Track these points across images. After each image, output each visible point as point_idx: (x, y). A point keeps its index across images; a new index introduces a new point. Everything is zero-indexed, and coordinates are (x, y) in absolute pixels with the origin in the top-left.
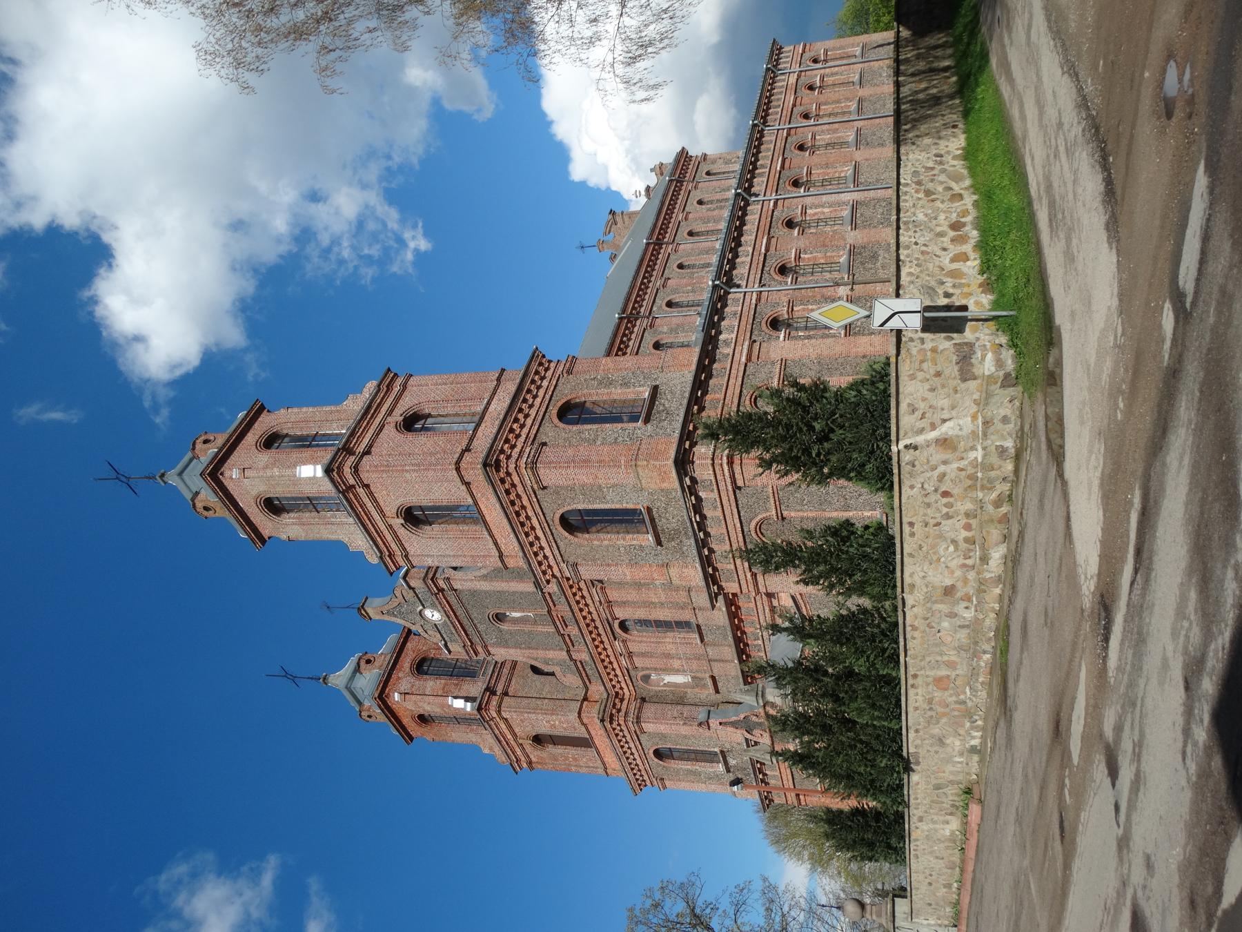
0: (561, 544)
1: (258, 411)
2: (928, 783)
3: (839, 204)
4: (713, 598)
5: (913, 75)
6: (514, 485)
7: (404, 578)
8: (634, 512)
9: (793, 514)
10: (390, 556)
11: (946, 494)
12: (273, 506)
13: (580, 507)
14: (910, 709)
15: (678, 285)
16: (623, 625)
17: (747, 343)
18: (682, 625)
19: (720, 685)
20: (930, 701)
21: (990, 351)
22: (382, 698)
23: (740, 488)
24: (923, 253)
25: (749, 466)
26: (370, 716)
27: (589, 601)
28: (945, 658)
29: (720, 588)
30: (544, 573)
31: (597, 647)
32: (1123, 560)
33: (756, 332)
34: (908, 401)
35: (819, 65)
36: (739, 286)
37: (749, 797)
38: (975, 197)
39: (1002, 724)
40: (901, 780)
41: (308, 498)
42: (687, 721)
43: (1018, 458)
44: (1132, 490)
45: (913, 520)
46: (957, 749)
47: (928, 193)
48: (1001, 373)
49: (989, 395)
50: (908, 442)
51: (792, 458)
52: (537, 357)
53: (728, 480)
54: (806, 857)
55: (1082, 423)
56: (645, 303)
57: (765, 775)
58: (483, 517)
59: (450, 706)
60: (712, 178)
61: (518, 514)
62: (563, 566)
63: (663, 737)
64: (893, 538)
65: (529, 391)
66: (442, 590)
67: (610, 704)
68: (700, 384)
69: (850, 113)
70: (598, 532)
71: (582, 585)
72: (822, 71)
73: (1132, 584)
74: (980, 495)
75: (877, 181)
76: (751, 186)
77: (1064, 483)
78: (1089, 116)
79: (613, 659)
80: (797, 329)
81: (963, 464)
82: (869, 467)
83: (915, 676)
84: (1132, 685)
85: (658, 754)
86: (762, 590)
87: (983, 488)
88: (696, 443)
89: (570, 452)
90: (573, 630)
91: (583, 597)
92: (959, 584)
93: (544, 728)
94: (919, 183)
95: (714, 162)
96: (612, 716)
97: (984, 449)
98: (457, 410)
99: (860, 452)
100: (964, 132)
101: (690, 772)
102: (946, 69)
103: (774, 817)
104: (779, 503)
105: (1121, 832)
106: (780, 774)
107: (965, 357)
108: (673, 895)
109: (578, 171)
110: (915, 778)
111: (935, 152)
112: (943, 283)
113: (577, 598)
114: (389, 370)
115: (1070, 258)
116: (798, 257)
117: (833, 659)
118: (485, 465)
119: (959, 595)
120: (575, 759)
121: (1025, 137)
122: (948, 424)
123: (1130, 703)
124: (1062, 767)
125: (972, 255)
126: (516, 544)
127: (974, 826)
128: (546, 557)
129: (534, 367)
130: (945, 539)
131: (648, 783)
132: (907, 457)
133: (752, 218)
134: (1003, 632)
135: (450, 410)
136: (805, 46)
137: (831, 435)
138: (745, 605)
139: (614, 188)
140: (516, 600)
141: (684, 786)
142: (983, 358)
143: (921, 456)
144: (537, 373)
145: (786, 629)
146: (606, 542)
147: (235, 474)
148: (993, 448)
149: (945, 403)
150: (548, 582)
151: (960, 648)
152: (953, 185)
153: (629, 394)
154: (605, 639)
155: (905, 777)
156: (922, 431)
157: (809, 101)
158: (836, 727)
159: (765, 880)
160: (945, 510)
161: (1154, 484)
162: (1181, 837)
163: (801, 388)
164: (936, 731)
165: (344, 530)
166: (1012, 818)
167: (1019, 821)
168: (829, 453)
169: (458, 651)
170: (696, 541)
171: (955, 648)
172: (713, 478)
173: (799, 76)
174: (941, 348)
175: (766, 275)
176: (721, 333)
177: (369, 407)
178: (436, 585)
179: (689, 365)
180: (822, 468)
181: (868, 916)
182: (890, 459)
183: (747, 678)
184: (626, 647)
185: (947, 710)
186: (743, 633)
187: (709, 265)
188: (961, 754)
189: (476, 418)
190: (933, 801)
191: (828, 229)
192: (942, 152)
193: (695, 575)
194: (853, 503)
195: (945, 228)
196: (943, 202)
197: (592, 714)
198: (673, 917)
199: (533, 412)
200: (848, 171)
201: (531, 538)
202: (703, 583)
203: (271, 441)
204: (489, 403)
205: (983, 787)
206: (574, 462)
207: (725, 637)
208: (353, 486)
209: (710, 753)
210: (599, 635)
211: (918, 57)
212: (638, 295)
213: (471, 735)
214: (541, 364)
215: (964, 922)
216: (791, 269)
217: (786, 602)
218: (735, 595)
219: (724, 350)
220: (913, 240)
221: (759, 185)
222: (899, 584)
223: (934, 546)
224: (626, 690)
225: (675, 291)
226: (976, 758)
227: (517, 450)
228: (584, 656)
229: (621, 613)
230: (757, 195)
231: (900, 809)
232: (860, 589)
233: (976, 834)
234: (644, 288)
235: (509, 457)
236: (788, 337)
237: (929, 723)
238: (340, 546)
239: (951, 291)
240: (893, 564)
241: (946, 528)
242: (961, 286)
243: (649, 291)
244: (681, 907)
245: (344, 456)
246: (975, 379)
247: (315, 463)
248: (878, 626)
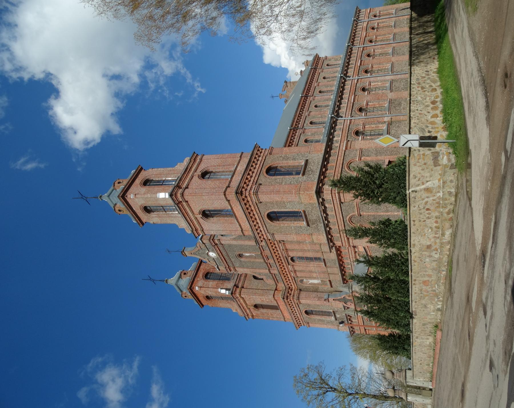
0: (267, 225)
1: (140, 170)
2: (420, 323)
3: (385, 81)
4: (331, 248)
5: (417, 34)
6: (248, 201)
7: (201, 239)
8: (297, 212)
9: (365, 214)
10: (196, 230)
11: (428, 209)
12: (147, 210)
13: (276, 210)
14: (413, 293)
15: (314, 115)
16: (292, 259)
17: (345, 142)
18: (317, 259)
19: (333, 284)
20: (421, 290)
21: (446, 155)
22: (191, 289)
23: (342, 203)
24: (420, 114)
25: (348, 196)
26: (186, 296)
27: (278, 249)
28: (427, 273)
29: (334, 244)
30: (260, 237)
31: (281, 268)
32: (489, 239)
33: (349, 137)
34: (413, 174)
35: (377, 18)
36: (342, 117)
37: (345, 329)
38: (442, 90)
39: (450, 299)
40: (409, 322)
41: (162, 206)
42: (319, 298)
43: (456, 196)
44: (492, 215)
45: (415, 219)
46: (432, 309)
47: (423, 88)
48: (450, 164)
49: (445, 172)
50: (413, 189)
51: (367, 194)
52: (257, 149)
53: (338, 200)
54: (368, 357)
55: (477, 188)
56: (301, 123)
57: (352, 321)
58: (235, 214)
59: (220, 293)
60: (329, 67)
61: (249, 213)
62: (268, 234)
63: (309, 305)
64: (407, 226)
65: (254, 162)
66: (217, 244)
67: (286, 292)
68: (326, 159)
69: (390, 39)
70: (283, 220)
71: (276, 242)
72: (378, 21)
73: (492, 247)
74: (441, 210)
75: (402, 70)
76: (347, 73)
77: (472, 209)
78: (482, 76)
79: (288, 273)
80: (366, 136)
81: (435, 198)
82: (397, 198)
83: (415, 280)
84: (491, 282)
85: (307, 312)
86: (351, 245)
87: (443, 207)
88: (324, 184)
89: (272, 188)
90: (271, 261)
91: (276, 247)
92: (433, 244)
93: (258, 302)
94: (419, 84)
95: (330, 60)
96: (287, 297)
97: (443, 192)
98: (223, 170)
99: (394, 193)
100: (438, 61)
101: (320, 320)
102: (431, 32)
103: (354, 340)
104: (359, 209)
105: (487, 334)
106: (358, 319)
107: (436, 157)
108: (313, 371)
109: (267, 59)
110: (415, 321)
111: (426, 70)
112: (428, 127)
113: (273, 248)
114: (194, 152)
115: (475, 126)
116: (367, 104)
117: (382, 273)
118: (236, 193)
119: (433, 248)
120: (272, 315)
121: (461, 72)
122: (429, 183)
123: (490, 289)
124: (470, 313)
125: (440, 115)
126: (249, 225)
127: (439, 340)
128: (261, 231)
129: (256, 151)
130: (428, 227)
131: (302, 324)
132: (412, 195)
133: (347, 87)
134: (450, 263)
135: (221, 170)
136: (370, 9)
137: (383, 186)
138: (344, 251)
139: (283, 66)
140: (247, 249)
141: (317, 326)
142: (443, 158)
143: (418, 195)
144: (257, 154)
145: (363, 262)
146: (286, 225)
147: (132, 196)
148: (447, 192)
149: (428, 175)
150: (262, 241)
151: (433, 269)
152: (433, 84)
153: (296, 163)
154: (284, 264)
155: (411, 320)
156: (418, 185)
157: (372, 34)
158: (383, 301)
159: (351, 365)
160: (427, 216)
161: (498, 214)
162: (503, 332)
163: (371, 167)
164: (423, 302)
165: (176, 219)
166: (453, 334)
167: (455, 336)
168: (381, 193)
169: (223, 269)
170: (324, 224)
171: (431, 269)
172: (331, 199)
173: (368, 23)
174: (426, 154)
175: (353, 112)
176: (334, 137)
177: (187, 168)
178: (214, 242)
179: (321, 151)
180: (379, 198)
181: (395, 377)
182: (406, 195)
183: (345, 281)
184: (294, 268)
185: (428, 294)
186: (343, 262)
187: (328, 106)
188: (434, 311)
189: (232, 173)
190: (422, 330)
191: (380, 92)
192: (428, 70)
193: (323, 238)
194: (391, 212)
195: (429, 103)
196: (428, 92)
197: (279, 296)
198: (313, 380)
199: (256, 171)
200: (389, 66)
201: (255, 223)
202: (327, 242)
203: (146, 183)
204: (237, 167)
205: (442, 324)
206: (273, 192)
207: (335, 264)
208: (181, 202)
209: (328, 312)
210: (282, 263)
211: (420, 26)
212: (298, 119)
213: (228, 304)
214: (258, 150)
215: (435, 379)
216: (364, 109)
217: (361, 249)
218: (339, 247)
219: (336, 145)
220: (416, 108)
221: (350, 72)
222: (409, 244)
223: (423, 229)
224: (293, 286)
225: (314, 117)
226: (439, 313)
227: (249, 187)
228: (276, 272)
229: (291, 254)
230: (349, 77)
231: (409, 333)
232: (393, 246)
233: (439, 343)
234: (300, 116)
235: (246, 190)
236: (363, 139)
237: (420, 299)
238: (175, 226)
239: (431, 130)
240: (407, 236)
241: (428, 223)
242: (435, 128)
243: (302, 117)
244: (316, 376)
245: (177, 190)
246: (440, 165)
247: (165, 192)
248: (400, 260)
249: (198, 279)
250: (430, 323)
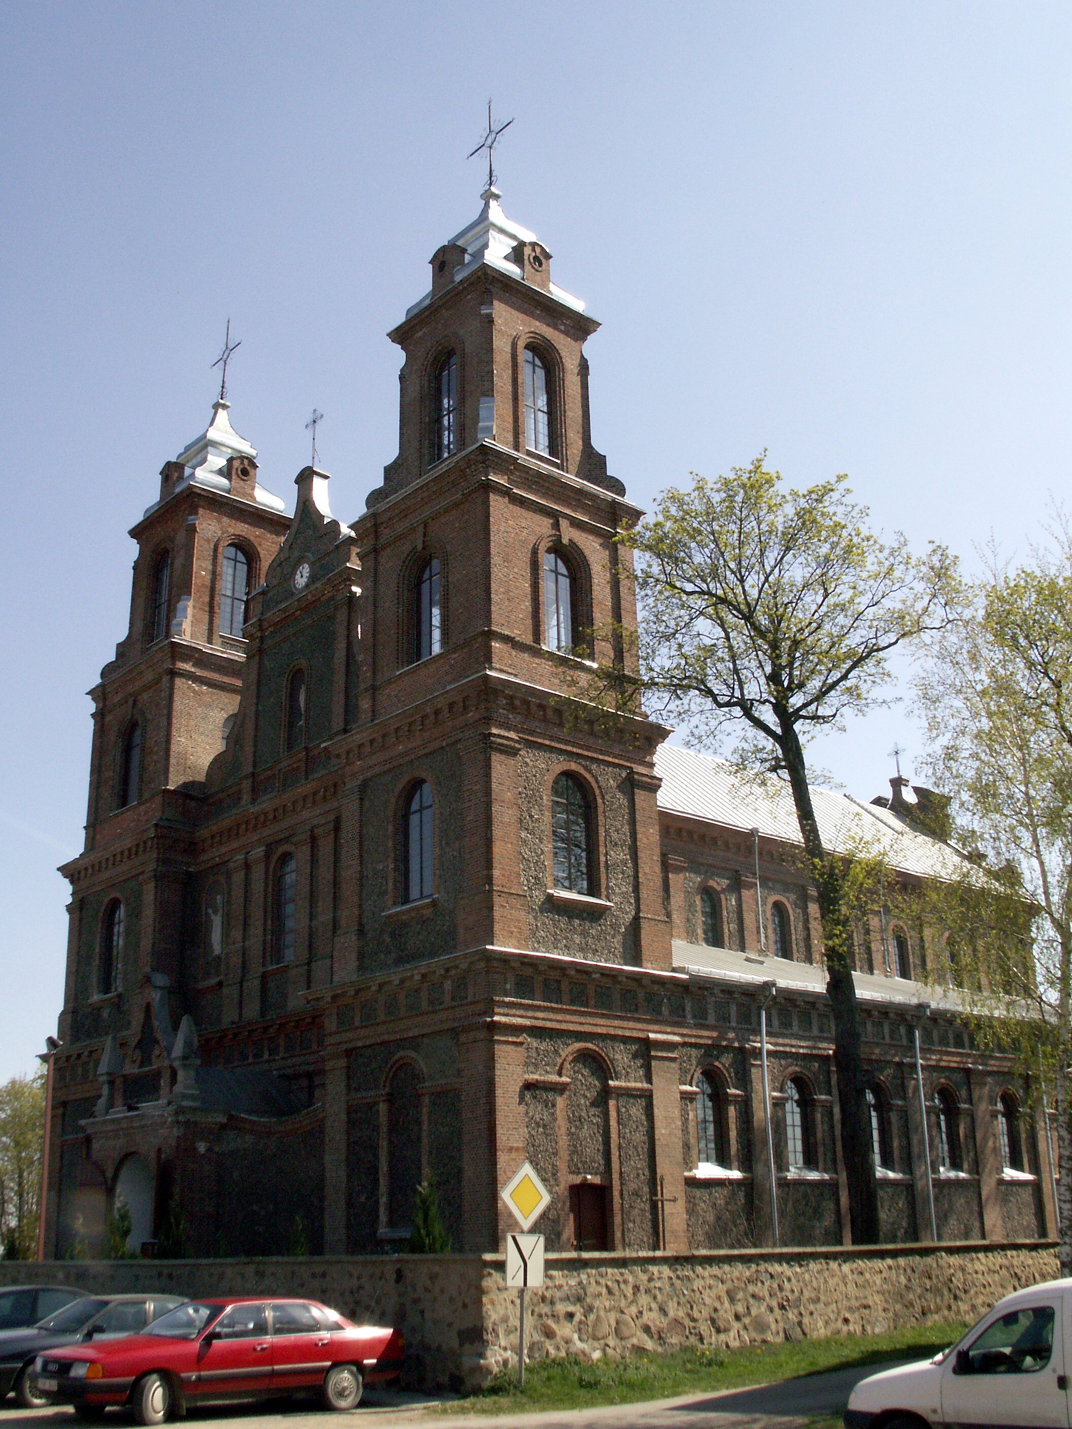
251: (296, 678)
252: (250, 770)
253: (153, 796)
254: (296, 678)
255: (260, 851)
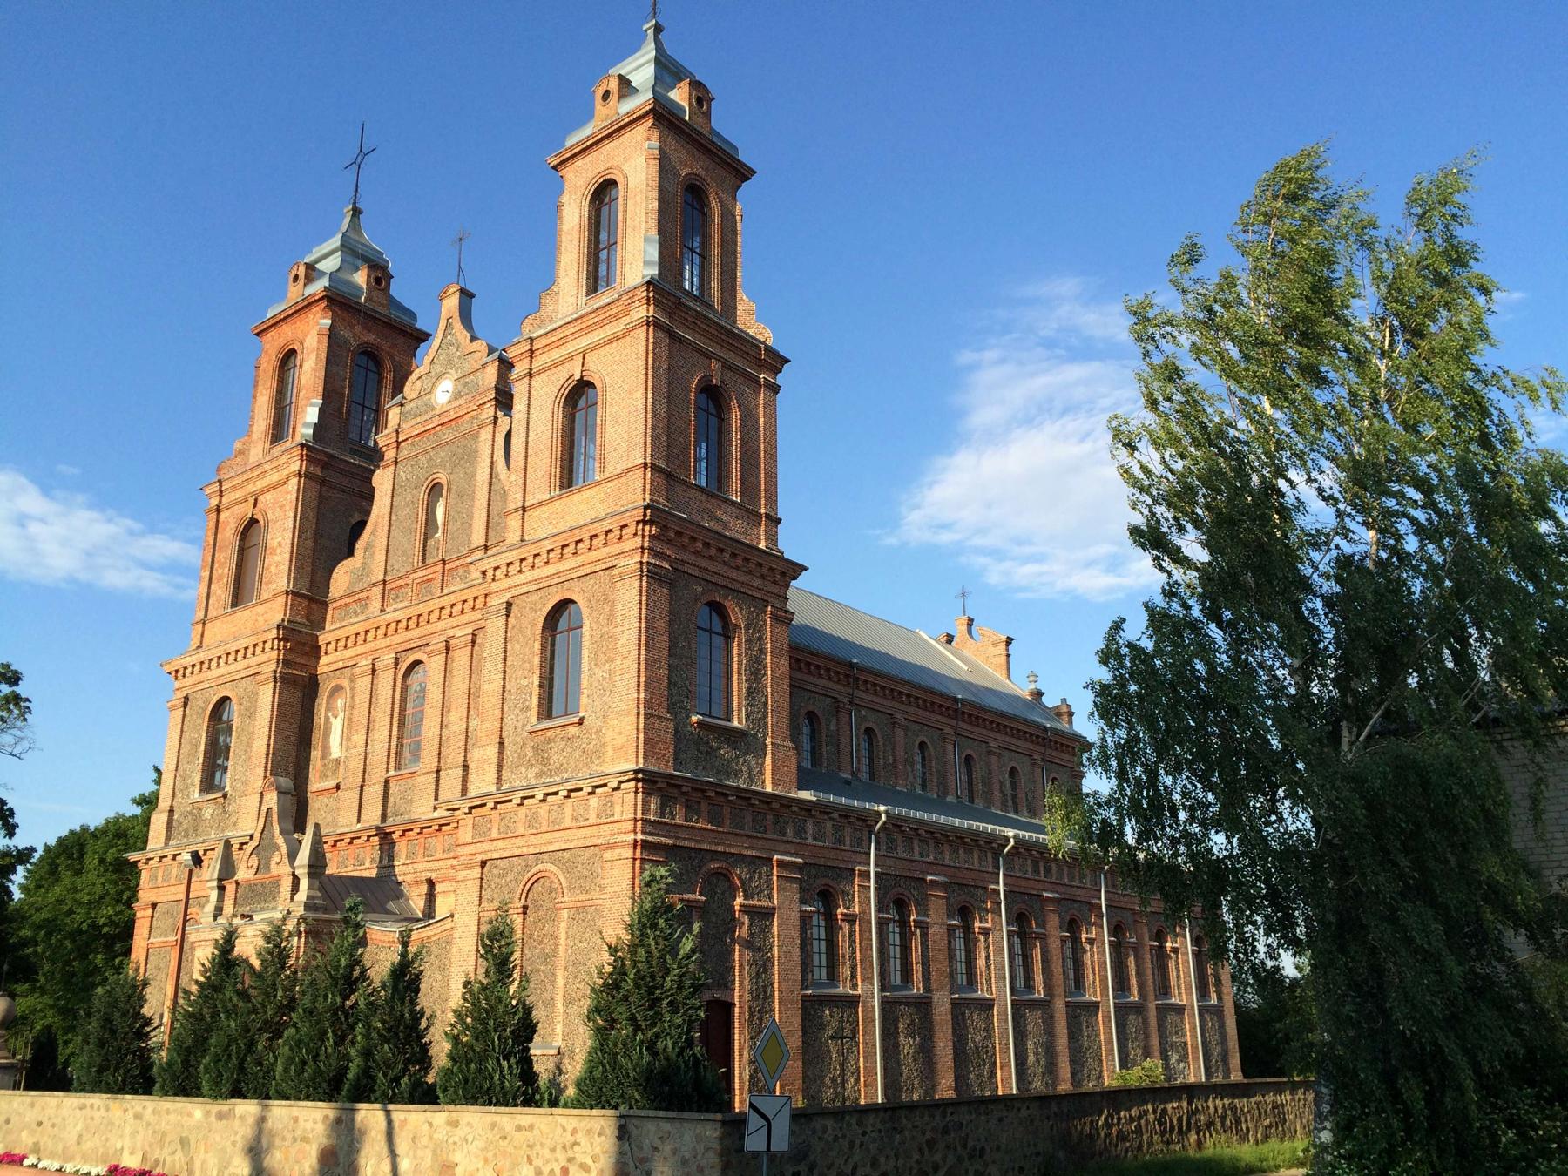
0: (535, 597)
9: (563, 925)
24: (852, 1144)
94: (946, 1131)
172: (616, 818)
249: (358, 328)
250: (190, 1163)
251: (435, 490)
252: (381, 577)
253: (275, 596)
254: (435, 490)
255: (387, 659)
